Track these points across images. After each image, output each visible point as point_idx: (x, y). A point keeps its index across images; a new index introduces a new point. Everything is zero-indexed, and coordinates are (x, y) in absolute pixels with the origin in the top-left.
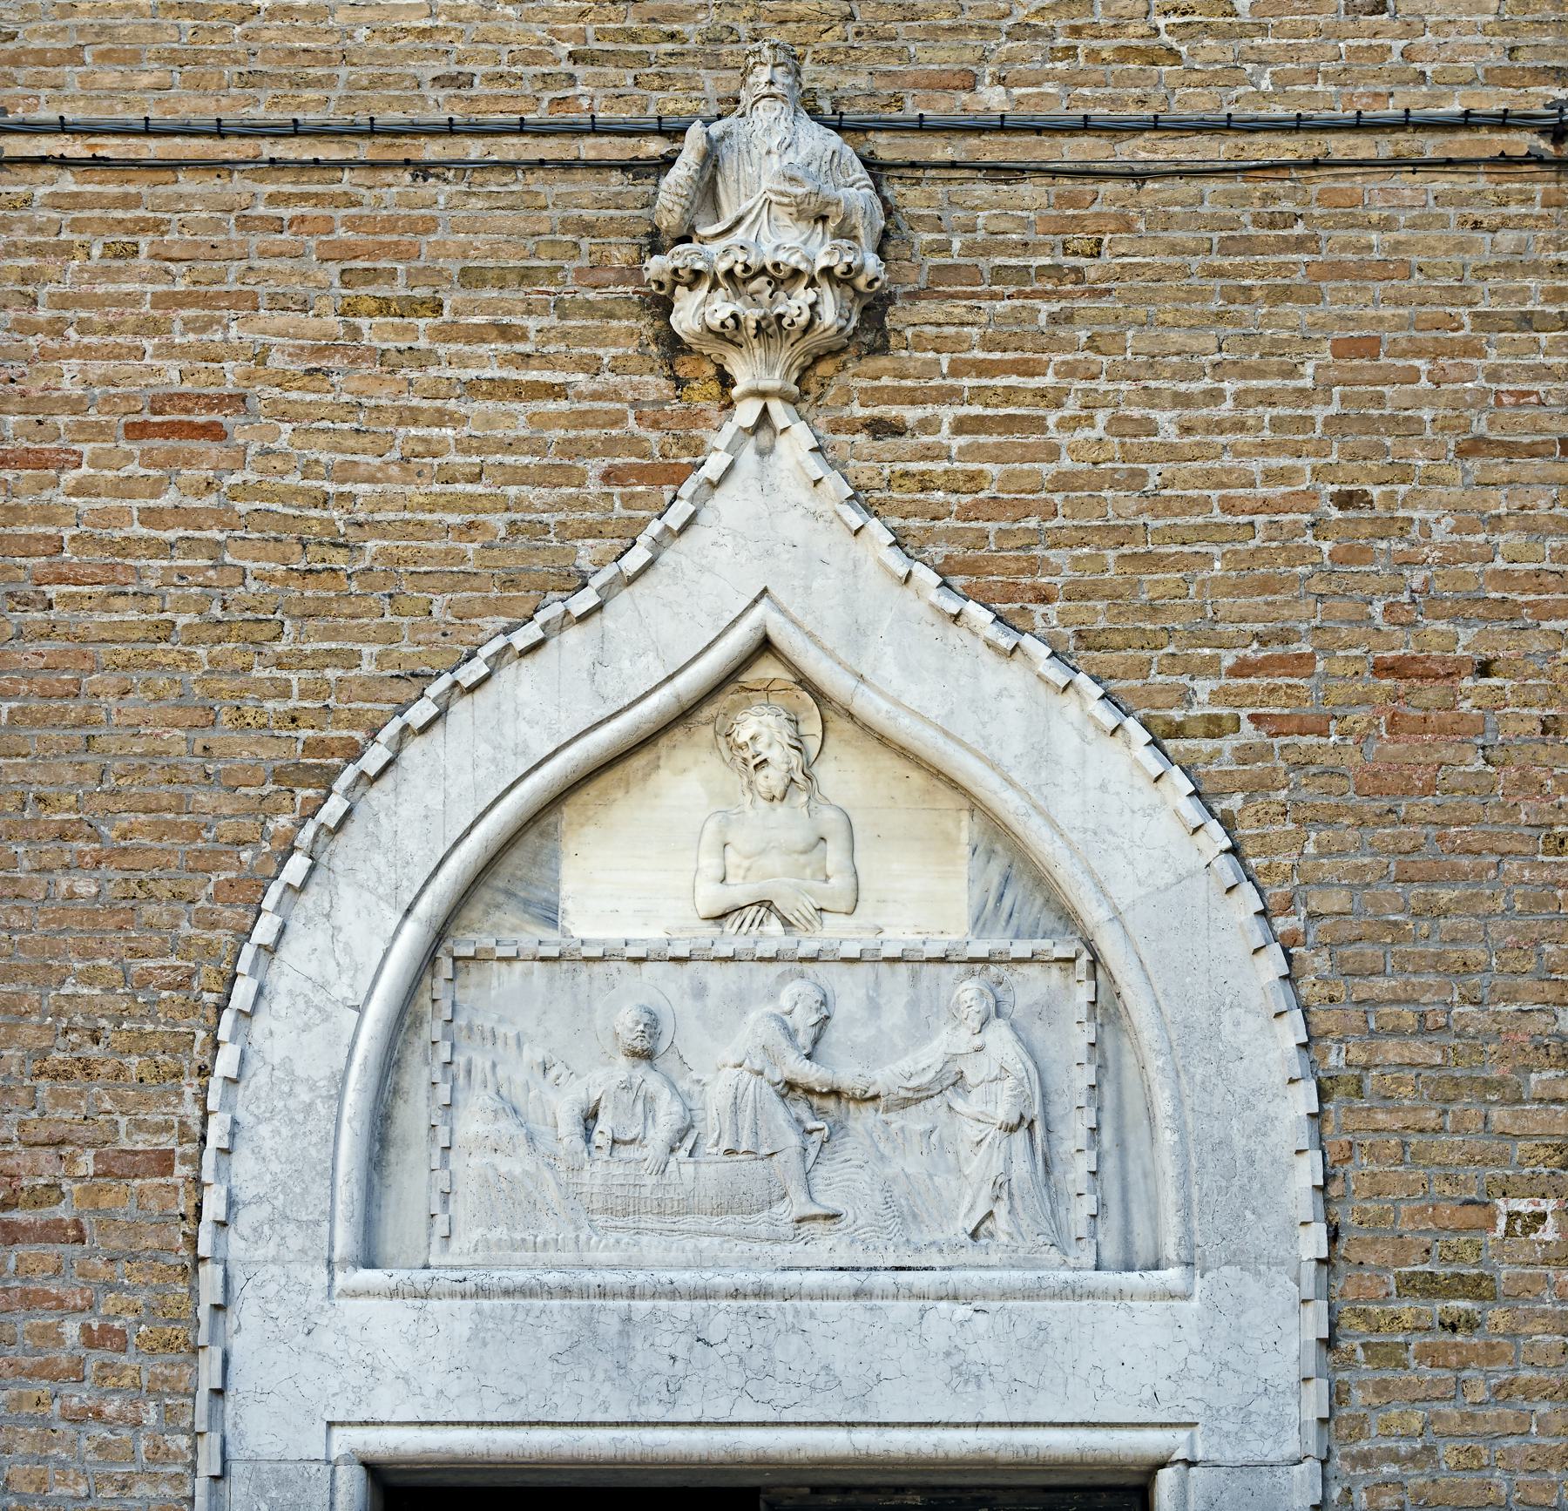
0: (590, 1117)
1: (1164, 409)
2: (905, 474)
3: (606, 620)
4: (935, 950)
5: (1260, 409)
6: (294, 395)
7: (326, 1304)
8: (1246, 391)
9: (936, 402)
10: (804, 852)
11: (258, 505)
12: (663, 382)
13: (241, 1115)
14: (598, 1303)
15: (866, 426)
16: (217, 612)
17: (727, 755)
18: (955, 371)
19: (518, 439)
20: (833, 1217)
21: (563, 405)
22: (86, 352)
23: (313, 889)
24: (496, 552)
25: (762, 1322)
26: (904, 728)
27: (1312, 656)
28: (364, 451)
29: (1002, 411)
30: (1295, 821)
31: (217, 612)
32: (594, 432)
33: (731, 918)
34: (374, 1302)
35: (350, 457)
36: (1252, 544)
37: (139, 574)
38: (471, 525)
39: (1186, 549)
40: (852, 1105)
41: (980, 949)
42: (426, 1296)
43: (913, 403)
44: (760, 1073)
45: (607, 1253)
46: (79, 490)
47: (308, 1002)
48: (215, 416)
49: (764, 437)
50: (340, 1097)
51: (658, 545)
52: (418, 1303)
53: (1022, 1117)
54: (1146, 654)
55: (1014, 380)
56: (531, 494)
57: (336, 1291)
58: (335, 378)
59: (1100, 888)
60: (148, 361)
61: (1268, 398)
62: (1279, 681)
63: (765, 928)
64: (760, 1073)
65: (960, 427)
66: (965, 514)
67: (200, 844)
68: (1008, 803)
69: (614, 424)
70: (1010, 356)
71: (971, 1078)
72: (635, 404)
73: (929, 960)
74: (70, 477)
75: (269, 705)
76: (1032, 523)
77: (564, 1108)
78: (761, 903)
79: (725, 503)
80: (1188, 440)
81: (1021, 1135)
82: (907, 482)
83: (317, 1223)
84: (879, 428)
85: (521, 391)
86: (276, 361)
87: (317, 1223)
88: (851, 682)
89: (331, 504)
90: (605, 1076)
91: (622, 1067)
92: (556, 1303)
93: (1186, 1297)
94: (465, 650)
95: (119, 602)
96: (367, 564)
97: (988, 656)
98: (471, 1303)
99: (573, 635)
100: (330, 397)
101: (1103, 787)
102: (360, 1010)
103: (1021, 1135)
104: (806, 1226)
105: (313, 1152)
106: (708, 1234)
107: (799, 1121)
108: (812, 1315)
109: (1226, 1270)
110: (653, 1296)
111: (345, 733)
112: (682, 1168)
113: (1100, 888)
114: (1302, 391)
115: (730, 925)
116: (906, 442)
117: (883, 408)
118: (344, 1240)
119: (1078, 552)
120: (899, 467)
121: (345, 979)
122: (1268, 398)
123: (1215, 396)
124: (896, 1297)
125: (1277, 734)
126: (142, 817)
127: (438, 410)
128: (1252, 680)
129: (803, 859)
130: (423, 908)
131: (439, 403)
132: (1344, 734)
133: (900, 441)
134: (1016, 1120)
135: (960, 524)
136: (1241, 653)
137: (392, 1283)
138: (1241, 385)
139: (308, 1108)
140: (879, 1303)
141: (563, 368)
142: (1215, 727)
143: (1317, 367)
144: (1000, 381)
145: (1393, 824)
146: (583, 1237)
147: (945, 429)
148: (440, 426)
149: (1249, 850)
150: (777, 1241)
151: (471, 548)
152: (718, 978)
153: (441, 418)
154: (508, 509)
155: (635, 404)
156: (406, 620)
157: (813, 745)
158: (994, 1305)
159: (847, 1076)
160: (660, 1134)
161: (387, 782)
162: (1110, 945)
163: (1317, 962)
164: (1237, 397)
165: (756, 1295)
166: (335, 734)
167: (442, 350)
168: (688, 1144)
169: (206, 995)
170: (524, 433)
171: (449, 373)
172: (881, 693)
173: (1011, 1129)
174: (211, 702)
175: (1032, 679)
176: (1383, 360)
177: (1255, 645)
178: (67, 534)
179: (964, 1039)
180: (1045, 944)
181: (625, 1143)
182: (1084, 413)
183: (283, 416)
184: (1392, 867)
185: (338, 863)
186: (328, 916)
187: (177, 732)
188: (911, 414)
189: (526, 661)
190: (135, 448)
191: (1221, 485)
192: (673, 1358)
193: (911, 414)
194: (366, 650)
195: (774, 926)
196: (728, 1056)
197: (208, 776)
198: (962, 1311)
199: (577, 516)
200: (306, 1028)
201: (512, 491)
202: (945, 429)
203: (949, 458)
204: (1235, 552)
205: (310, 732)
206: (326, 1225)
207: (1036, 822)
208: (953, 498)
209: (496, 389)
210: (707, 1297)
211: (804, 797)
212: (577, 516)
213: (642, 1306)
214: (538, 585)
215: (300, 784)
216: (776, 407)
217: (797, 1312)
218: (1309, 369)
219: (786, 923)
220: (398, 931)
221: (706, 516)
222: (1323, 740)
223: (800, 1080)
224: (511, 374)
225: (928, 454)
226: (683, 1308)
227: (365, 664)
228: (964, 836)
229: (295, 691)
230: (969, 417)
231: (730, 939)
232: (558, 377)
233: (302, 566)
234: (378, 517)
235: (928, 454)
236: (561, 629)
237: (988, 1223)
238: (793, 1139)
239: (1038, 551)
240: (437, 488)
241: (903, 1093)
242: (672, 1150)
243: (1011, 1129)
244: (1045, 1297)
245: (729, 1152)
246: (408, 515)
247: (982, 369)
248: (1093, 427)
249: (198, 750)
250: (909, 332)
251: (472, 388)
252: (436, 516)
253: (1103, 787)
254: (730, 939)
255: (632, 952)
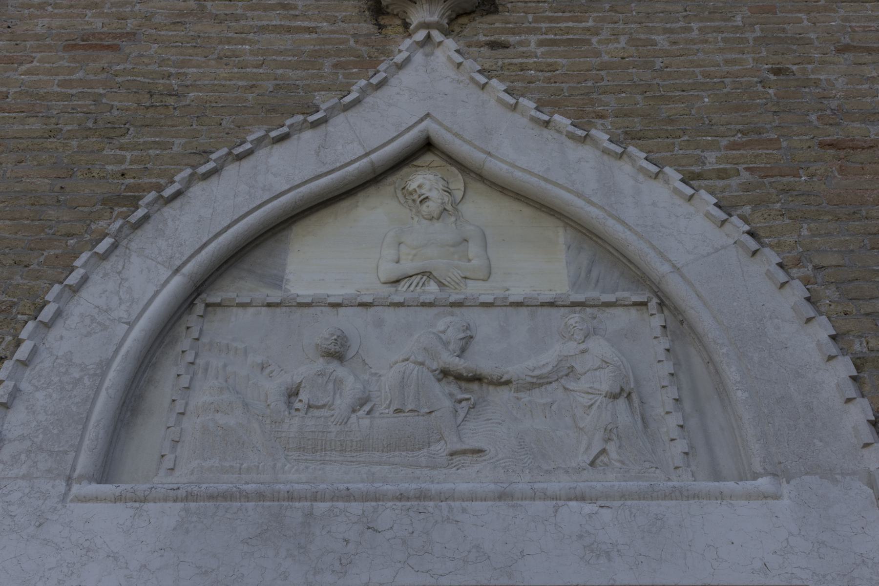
0: (293, 393)
1: (659, 35)
2: (510, 64)
3: (330, 127)
4: (547, 297)
5: (715, 34)
6: (163, 33)
7: (59, 506)
8: (705, 27)
9: (527, 33)
10: (453, 246)
11: (129, 78)
12: (371, 26)
13: (24, 386)
14: (286, 504)
15: (487, 44)
16: (90, 124)
17: (402, 200)
18: (536, 20)
19: (286, 49)
20: (479, 451)
21: (314, 36)
22: (52, 16)
23: (113, 258)
24: (266, 97)
25: (422, 516)
26: (520, 178)
27: (778, 139)
28: (197, 55)
29: (564, 37)
30: (790, 218)
31: (90, 124)
32: (330, 47)
33: (402, 283)
34: (99, 506)
35: (188, 57)
36: (725, 90)
37: (49, 108)
38: (252, 87)
39: (685, 93)
40: (491, 388)
41: (580, 298)
42: (145, 500)
43: (514, 34)
44: (422, 364)
45: (295, 475)
46: (28, 72)
47: (93, 320)
48: (116, 42)
49: (428, 49)
50: (103, 375)
51: (363, 91)
52: (137, 505)
53: (622, 390)
54: (670, 140)
55: (570, 24)
56: (290, 73)
57: (71, 497)
58: (188, 25)
59: (662, 255)
60: (87, 19)
61: (718, 30)
62: (760, 152)
63: (427, 288)
64: (422, 364)
65: (541, 44)
66: (548, 80)
67: (42, 235)
68: (592, 214)
69: (341, 44)
70: (567, 14)
71: (579, 368)
72: (354, 35)
73: (543, 305)
74: (24, 68)
75: (109, 168)
76: (590, 84)
77: (272, 387)
78: (423, 273)
79: (406, 77)
80: (674, 47)
81: (622, 403)
82: (512, 67)
83: (66, 453)
84: (494, 45)
85: (289, 30)
86: (158, 19)
87: (66, 453)
88: (483, 156)
89: (172, 78)
90: (304, 369)
91: (320, 364)
92: (251, 505)
93: (777, 497)
94: (239, 141)
95: (32, 120)
96: (188, 103)
97: (570, 143)
98: (180, 505)
99: (308, 135)
100: (183, 33)
101: (654, 204)
102: (131, 325)
103: (622, 403)
104: (457, 459)
105: (74, 408)
106: (379, 463)
107: (451, 395)
108: (464, 511)
109: (807, 478)
110: (332, 500)
111: (154, 180)
112: (361, 423)
113: (662, 255)
114: (737, 26)
115: (403, 286)
116: (511, 51)
117: (497, 36)
118: (85, 462)
119: (619, 96)
120: (506, 61)
121: (123, 307)
122: (718, 30)
123: (688, 30)
124: (533, 499)
125: (766, 177)
126: (8, 222)
127: (242, 38)
128: (742, 151)
129: (452, 249)
130: (188, 269)
131: (243, 35)
132: (811, 176)
133: (507, 50)
134: (618, 391)
135: (545, 85)
136: (732, 139)
137: (118, 491)
138: (701, 24)
139: (77, 382)
140: (519, 502)
141: (315, 20)
142: (722, 174)
143: (743, 18)
144: (563, 25)
145: (859, 220)
146: (279, 465)
147: (533, 44)
148: (242, 45)
149: (762, 234)
150: (434, 467)
151: (250, 96)
152: (390, 315)
153: (243, 42)
154: (276, 79)
155: (354, 35)
156: (204, 128)
157: (459, 195)
158: (617, 503)
159: (485, 365)
160: (342, 403)
161: (177, 203)
162: (675, 287)
163: (828, 293)
164: (700, 29)
165: (418, 498)
166: (148, 180)
167: (249, 14)
168: (367, 408)
169: (19, 316)
170: (290, 47)
171: (252, 23)
172: (502, 161)
173: (615, 397)
174: (73, 166)
175: (598, 153)
176: (779, 15)
177: (740, 135)
178: (12, 91)
179: (572, 347)
180: (626, 294)
181: (318, 407)
182: (613, 37)
183: (155, 41)
184: (866, 241)
185: (133, 245)
186: (119, 273)
187: (46, 181)
188: (512, 39)
189: (277, 147)
190: (66, 55)
191: (701, 66)
192: (347, 541)
193: (512, 39)
194: (177, 141)
195: (433, 287)
196: (395, 354)
197: (58, 201)
198: (588, 508)
199: (317, 82)
200: (89, 334)
201: (280, 71)
202: (533, 44)
203: (536, 57)
204: (716, 94)
205: (132, 181)
206: (72, 454)
207: (611, 222)
208: (540, 74)
209: (275, 29)
210: (377, 499)
211: (453, 219)
212: (317, 82)
213: (322, 507)
214: (289, 109)
215: (118, 205)
216: (437, 35)
217: (451, 509)
218: (739, 18)
219: (441, 284)
220: (167, 281)
221: (393, 81)
222: (797, 179)
223: (452, 368)
224: (287, 23)
225: (523, 55)
226: (356, 508)
227: (175, 149)
228: (561, 240)
229: (128, 160)
230: (546, 39)
231: (402, 293)
232: (313, 24)
233: (148, 104)
234: (198, 83)
235: (523, 55)
236: (300, 131)
237: (602, 458)
238: (447, 403)
239: (594, 96)
240: (236, 70)
241: (529, 379)
242: (354, 411)
243: (615, 397)
244: (658, 498)
245: (398, 411)
246: (216, 82)
247: (551, 20)
248: (619, 43)
249: (57, 188)
250: (509, 5)
251: (263, 29)
252: (232, 82)
253: (654, 204)
254: (402, 293)
255: (331, 300)
